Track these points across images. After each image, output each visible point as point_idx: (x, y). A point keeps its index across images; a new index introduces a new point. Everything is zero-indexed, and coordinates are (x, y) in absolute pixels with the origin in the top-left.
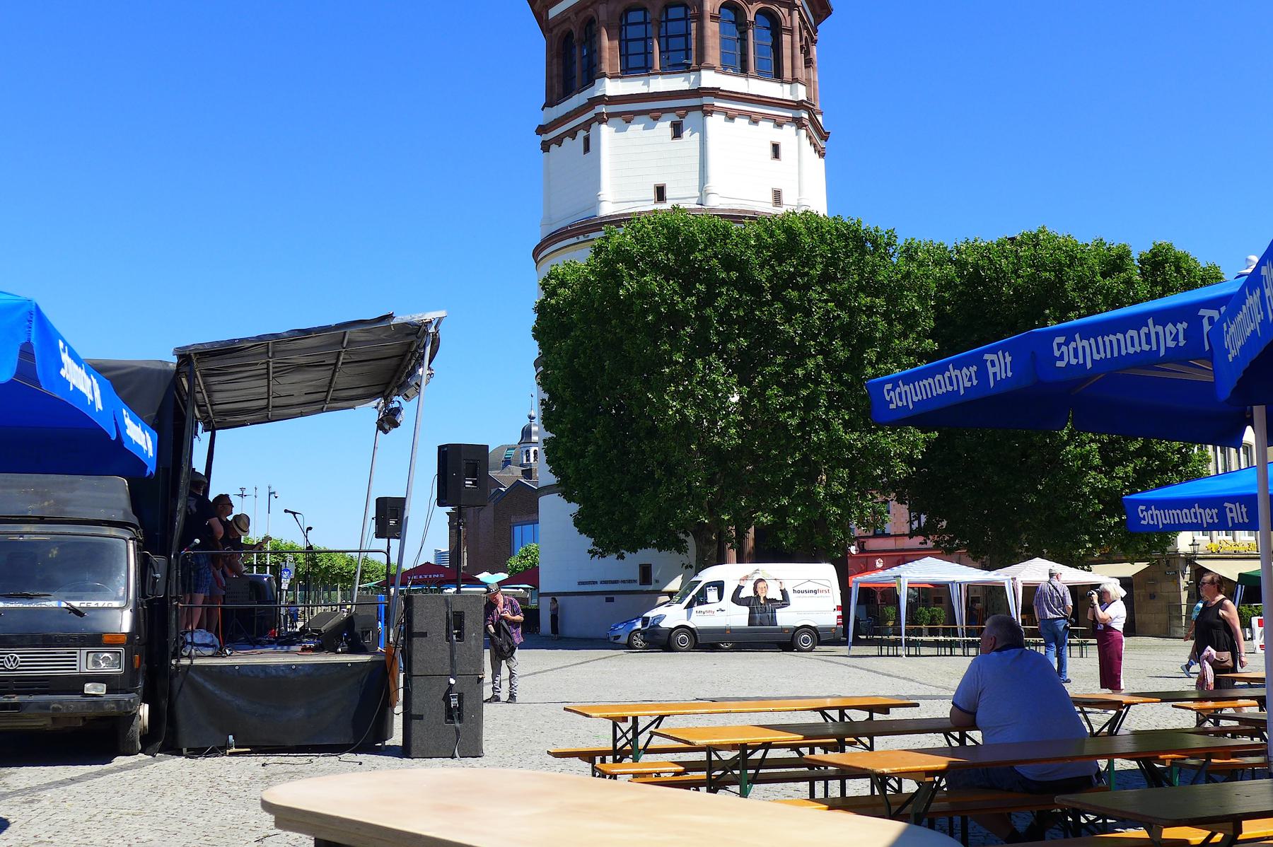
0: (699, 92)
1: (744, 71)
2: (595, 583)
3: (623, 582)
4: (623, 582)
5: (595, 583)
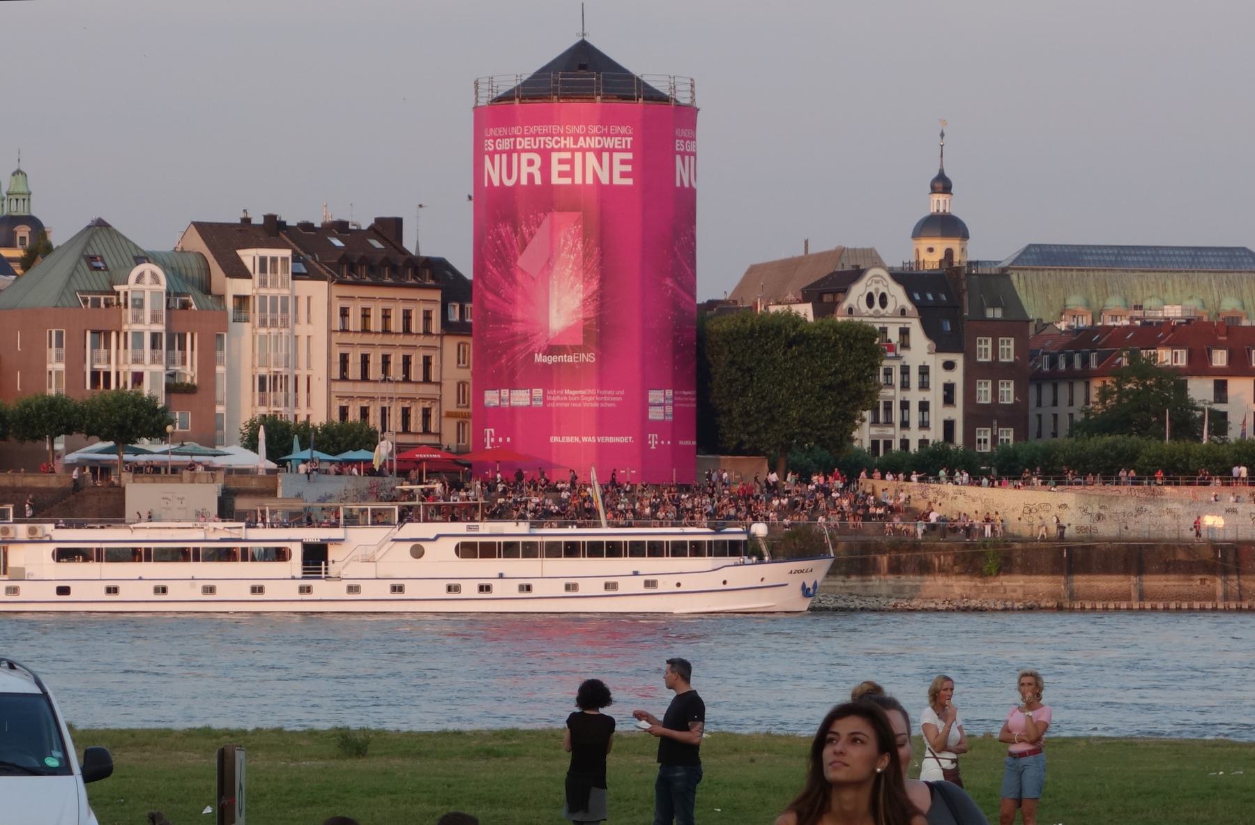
2: (150, 528)
3: (145, 528)
4: (145, 528)
5: (150, 528)
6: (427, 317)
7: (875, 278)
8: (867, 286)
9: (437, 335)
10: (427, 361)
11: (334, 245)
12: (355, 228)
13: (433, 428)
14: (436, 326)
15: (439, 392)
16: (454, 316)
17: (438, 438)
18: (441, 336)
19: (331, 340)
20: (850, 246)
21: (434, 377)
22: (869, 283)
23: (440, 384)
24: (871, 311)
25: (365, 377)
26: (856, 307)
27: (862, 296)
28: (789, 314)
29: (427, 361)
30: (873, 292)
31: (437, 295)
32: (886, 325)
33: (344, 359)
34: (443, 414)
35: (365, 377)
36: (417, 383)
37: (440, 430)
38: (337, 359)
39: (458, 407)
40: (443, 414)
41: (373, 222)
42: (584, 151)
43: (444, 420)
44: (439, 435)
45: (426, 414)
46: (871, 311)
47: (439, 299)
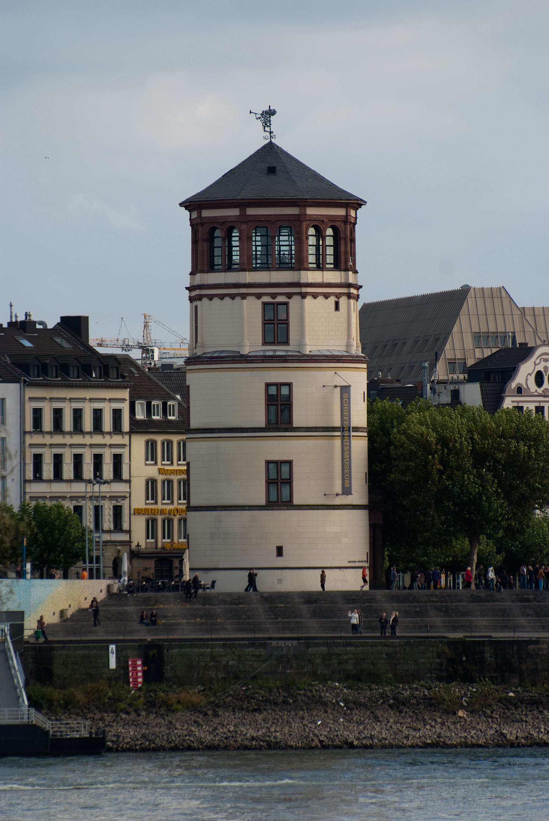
0: (299, 285)
1: (191, 569)
2: (355, 562)
3: (359, 562)
5: (355, 562)
6: (117, 413)
7: (544, 357)
8: (535, 364)
9: (126, 433)
10: (117, 459)
11: (23, 346)
12: (41, 327)
13: (126, 526)
14: (126, 426)
15: (129, 490)
16: (140, 415)
17: (128, 536)
18: (131, 432)
19: (24, 442)
20: (189, 223)
21: (125, 476)
22: (537, 362)
23: (129, 481)
24: (540, 390)
25: (78, 476)
26: (525, 386)
27: (530, 374)
28: (128, 355)
29: (117, 459)
30: (542, 370)
31: (125, 394)
32: (542, 404)
33: (38, 459)
34: (132, 512)
35: (78, 476)
36: (49, 481)
37: (130, 527)
38: (29, 460)
39: (146, 504)
40: (132, 512)
41: (59, 321)
42: (279, 241)
43: (132, 517)
44: (129, 532)
45: (118, 511)
46: (540, 390)
47: (127, 398)
